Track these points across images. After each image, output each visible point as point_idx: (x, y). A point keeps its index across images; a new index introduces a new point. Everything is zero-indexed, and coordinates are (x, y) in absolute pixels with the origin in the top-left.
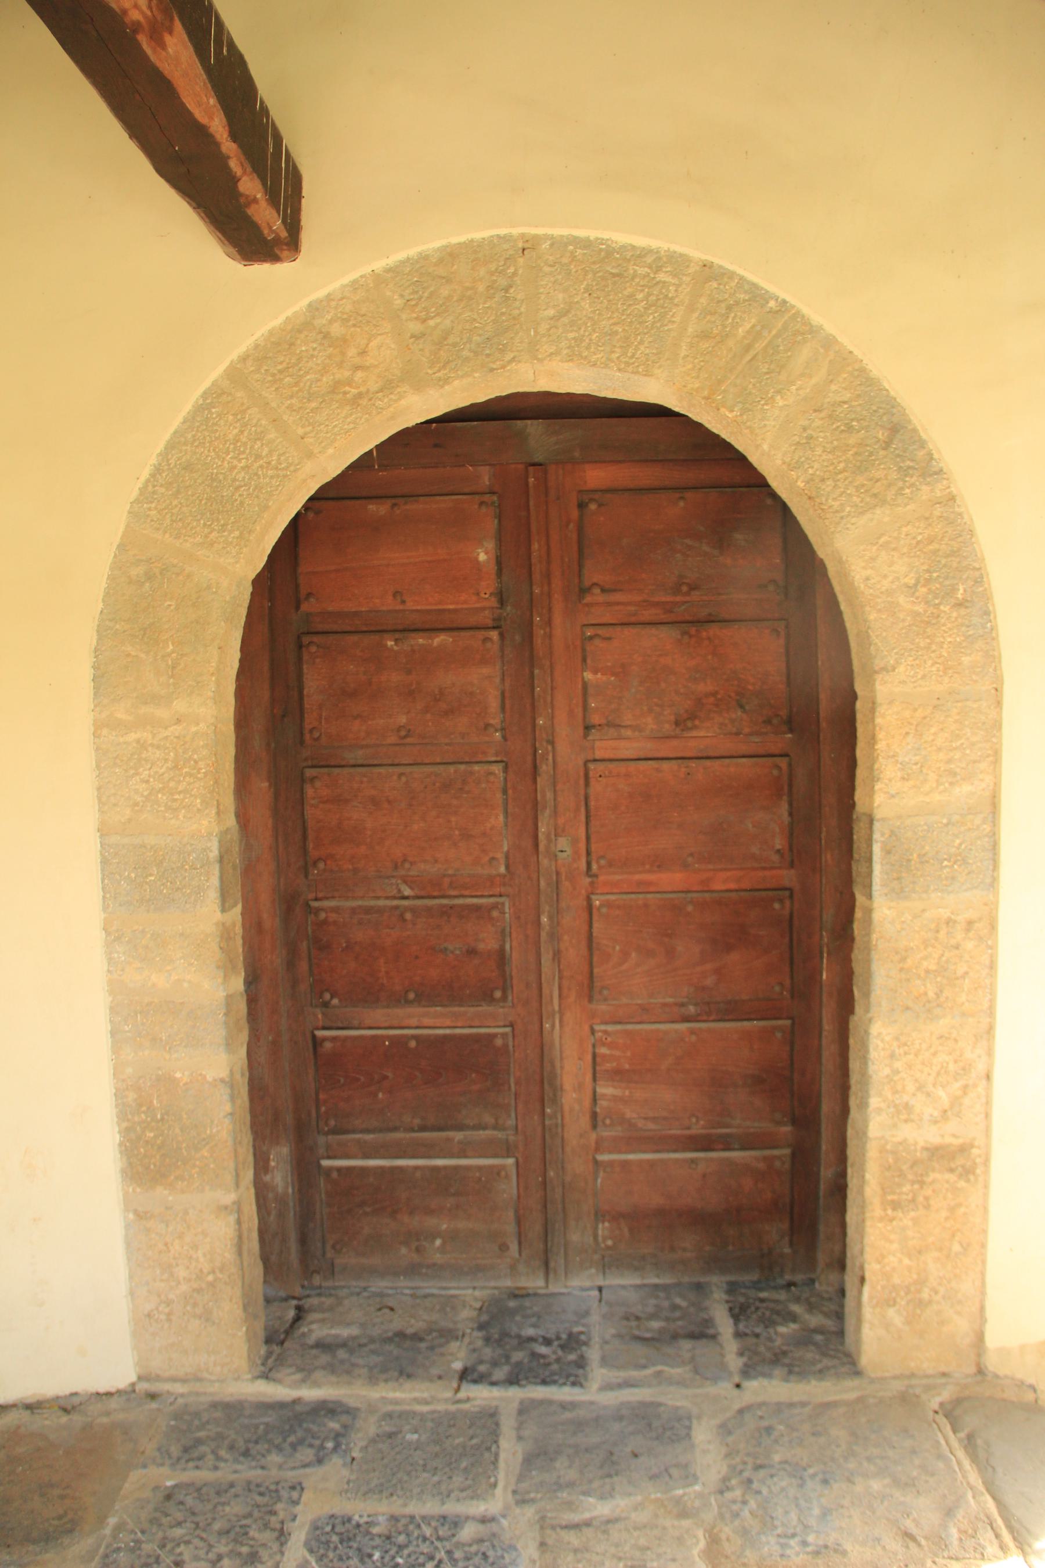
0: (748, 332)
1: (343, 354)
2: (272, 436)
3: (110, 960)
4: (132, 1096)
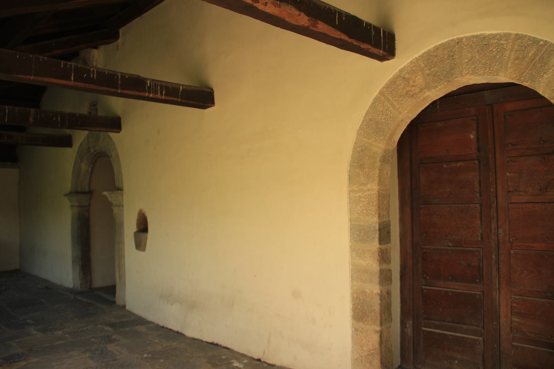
0: (533, 54)
1: (409, 83)
2: (391, 109)
3: (352, 256)
4: (355, 295)
